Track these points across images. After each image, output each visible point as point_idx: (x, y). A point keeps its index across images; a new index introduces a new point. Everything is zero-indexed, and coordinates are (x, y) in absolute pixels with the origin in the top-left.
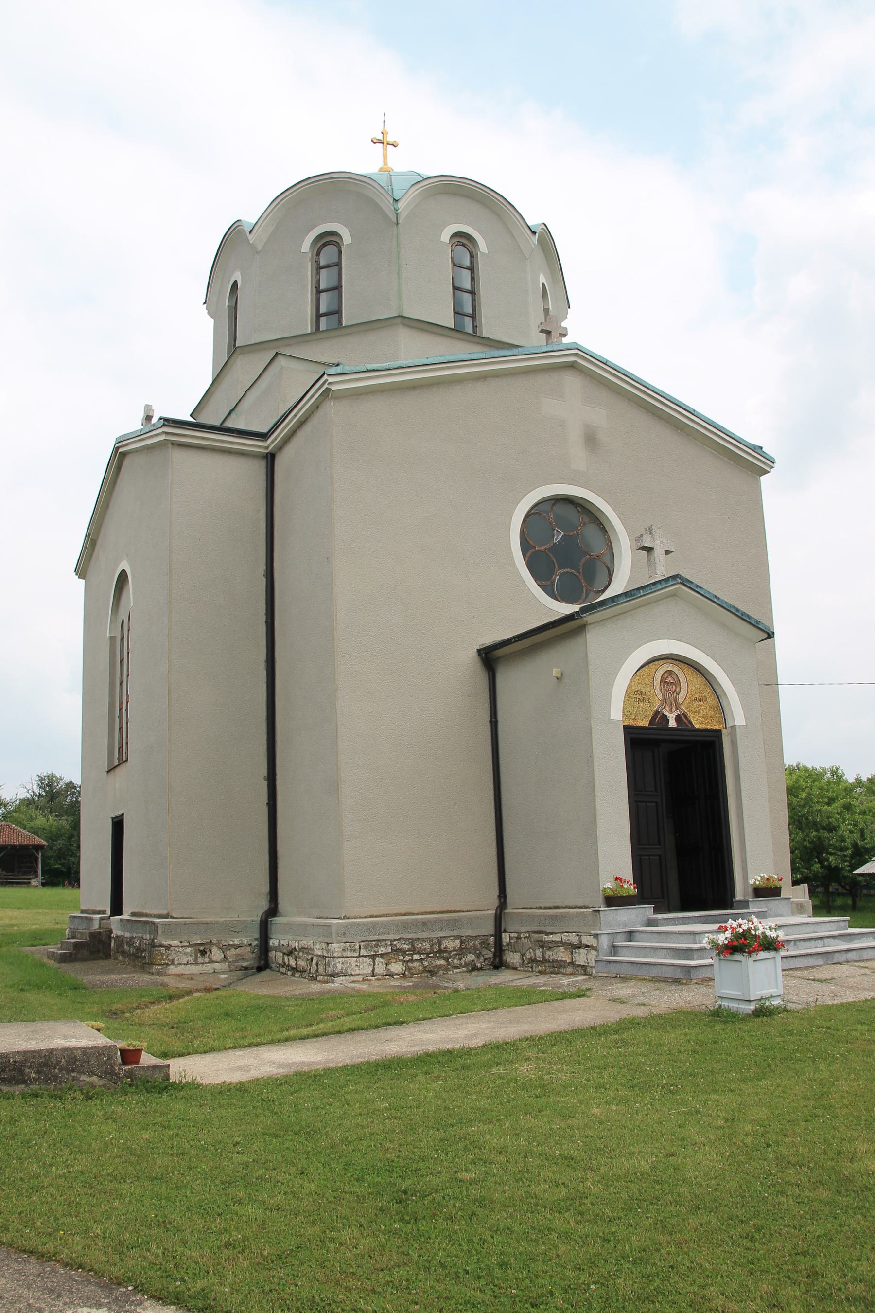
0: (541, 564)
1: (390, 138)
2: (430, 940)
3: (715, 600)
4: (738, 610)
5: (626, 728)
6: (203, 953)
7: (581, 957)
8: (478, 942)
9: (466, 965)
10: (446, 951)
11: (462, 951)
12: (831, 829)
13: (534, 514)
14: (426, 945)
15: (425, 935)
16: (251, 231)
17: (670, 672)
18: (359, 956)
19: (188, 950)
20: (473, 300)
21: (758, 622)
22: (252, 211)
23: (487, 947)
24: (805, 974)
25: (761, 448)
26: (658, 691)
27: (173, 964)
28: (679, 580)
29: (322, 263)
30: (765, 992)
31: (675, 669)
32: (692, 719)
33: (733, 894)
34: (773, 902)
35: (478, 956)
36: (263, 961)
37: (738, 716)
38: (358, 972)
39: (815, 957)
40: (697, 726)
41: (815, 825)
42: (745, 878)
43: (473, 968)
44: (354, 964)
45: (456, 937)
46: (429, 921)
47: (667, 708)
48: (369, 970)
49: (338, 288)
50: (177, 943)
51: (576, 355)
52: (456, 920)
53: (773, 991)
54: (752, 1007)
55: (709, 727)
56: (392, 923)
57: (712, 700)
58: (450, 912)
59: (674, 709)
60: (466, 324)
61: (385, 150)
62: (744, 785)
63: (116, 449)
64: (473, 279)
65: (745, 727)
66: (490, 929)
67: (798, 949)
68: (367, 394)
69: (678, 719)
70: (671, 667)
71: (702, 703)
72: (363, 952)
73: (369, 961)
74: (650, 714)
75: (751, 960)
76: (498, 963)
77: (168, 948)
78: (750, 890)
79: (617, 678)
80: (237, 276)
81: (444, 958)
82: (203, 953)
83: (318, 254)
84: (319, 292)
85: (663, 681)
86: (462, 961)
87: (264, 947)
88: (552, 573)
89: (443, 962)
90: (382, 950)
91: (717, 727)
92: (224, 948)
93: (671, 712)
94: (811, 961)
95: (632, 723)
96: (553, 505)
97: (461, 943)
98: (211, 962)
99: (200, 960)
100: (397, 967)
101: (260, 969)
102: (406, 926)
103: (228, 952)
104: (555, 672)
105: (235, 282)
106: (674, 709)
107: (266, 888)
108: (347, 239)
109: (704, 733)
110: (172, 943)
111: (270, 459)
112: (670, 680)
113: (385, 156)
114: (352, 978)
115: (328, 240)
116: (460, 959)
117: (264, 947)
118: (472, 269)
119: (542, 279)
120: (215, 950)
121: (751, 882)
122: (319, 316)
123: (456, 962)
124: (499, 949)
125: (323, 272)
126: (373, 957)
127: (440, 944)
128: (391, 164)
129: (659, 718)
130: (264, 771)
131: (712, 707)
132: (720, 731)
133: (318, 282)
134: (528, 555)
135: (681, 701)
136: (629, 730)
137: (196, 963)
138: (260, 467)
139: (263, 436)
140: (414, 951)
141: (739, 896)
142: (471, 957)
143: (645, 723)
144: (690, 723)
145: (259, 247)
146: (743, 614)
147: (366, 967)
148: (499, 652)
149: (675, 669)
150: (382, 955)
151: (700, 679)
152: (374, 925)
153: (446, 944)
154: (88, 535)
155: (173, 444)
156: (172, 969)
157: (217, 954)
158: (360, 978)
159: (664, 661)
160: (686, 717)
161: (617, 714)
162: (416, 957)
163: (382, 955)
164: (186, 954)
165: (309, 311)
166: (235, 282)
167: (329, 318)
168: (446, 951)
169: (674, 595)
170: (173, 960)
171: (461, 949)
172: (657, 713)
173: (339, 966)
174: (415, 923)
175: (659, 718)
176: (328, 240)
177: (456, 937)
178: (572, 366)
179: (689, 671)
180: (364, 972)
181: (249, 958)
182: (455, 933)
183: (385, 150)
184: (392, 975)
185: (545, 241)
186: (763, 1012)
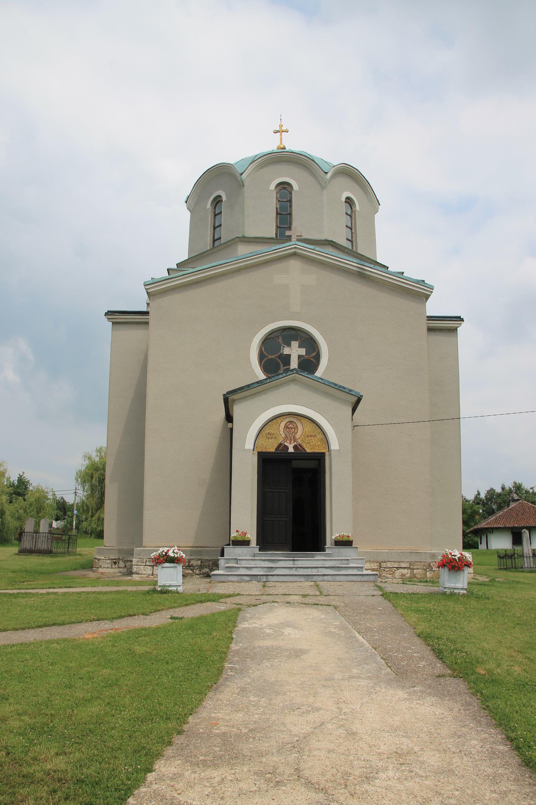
1: (284, 128)
3: (320, 380)
4: (336, 385)
8: (210, 563)
9: (203, 574)
10: (192, 566)
11: (201, 567)
13: (269, 338)
16: (242, 174)
18: (146, 565)
19: (108, 561)
21: (350, 390)
25: (423, 281)
27: (101, 567)
28: (295, 372)
30: (168, 583)
31: (295, 420)
32: (305, 447)
33: (325, 544)
34: (344, 549)
37: (334, 445)
38: (144, 573)
39: (299, 577)
40: (308, 451)
42: (332, 535)
44: (143, 569)
45: (198, 560)
47: (288, 441)
48: (151, 572)
50: (103, 558)
51: (295, 248)
52: (199, 551)
55: (317, 451)
57: (321, 436)
58: (202, 547)
59: (292, 442)
61: (281, 135)
62: (334, 483)
67: (298, 572)
68: (169, 290)
69: (295, 447)
70: (288, 420)
71: (312, 438)
72: (148, 563)
73: (150, 568)
77: (99, 560)
78: (333, 542)
81: (191, 570)
82: (115, 563)
83: (215, 208)
85: (286, 427)
86: (201, 572)
89: (190, 571)
91: (323, 451)
93: (290, 443)
95: (264, 450)
96: (283, 332)
97: (201, 562)
98: (119, 567)
99: (113, 566)
103: (127, 564)
106: (292, 442)
108: (224, 198)
109: (312, 455)
110: (101, 558)
112: (291, 426)
113: (281, 139)
114: (141, 576)
115: (284, 187)
116: (200, 571)
120: (121, 562)
123: (198, 572)
126: (153, 566)
127: (189, 562)
128: (285, 143)
129: (282, 447)
132: (324, 453)
134: (263, 361)
135: (297, 437)
137: (112, 568)
143: (273, 450)
144: (304, 449)
146: (340, 386)
149: (295, 420)
153: (192, 562)
156: (101, 570)
158: (146, 576)
159: (287, 416)
160: (301, 446)
161: (249, 445)
164: (107, 563)
168: (192, 566)
169: (293, 381)
170: (101, 566)
171: (201, 565)
172: (281, 444)
176: (349, 201)
177: (198, 560)
178: (294, 255)
179: (268, 426)
180: (147, 573)
182: (199, 557)
183: (281, 135)
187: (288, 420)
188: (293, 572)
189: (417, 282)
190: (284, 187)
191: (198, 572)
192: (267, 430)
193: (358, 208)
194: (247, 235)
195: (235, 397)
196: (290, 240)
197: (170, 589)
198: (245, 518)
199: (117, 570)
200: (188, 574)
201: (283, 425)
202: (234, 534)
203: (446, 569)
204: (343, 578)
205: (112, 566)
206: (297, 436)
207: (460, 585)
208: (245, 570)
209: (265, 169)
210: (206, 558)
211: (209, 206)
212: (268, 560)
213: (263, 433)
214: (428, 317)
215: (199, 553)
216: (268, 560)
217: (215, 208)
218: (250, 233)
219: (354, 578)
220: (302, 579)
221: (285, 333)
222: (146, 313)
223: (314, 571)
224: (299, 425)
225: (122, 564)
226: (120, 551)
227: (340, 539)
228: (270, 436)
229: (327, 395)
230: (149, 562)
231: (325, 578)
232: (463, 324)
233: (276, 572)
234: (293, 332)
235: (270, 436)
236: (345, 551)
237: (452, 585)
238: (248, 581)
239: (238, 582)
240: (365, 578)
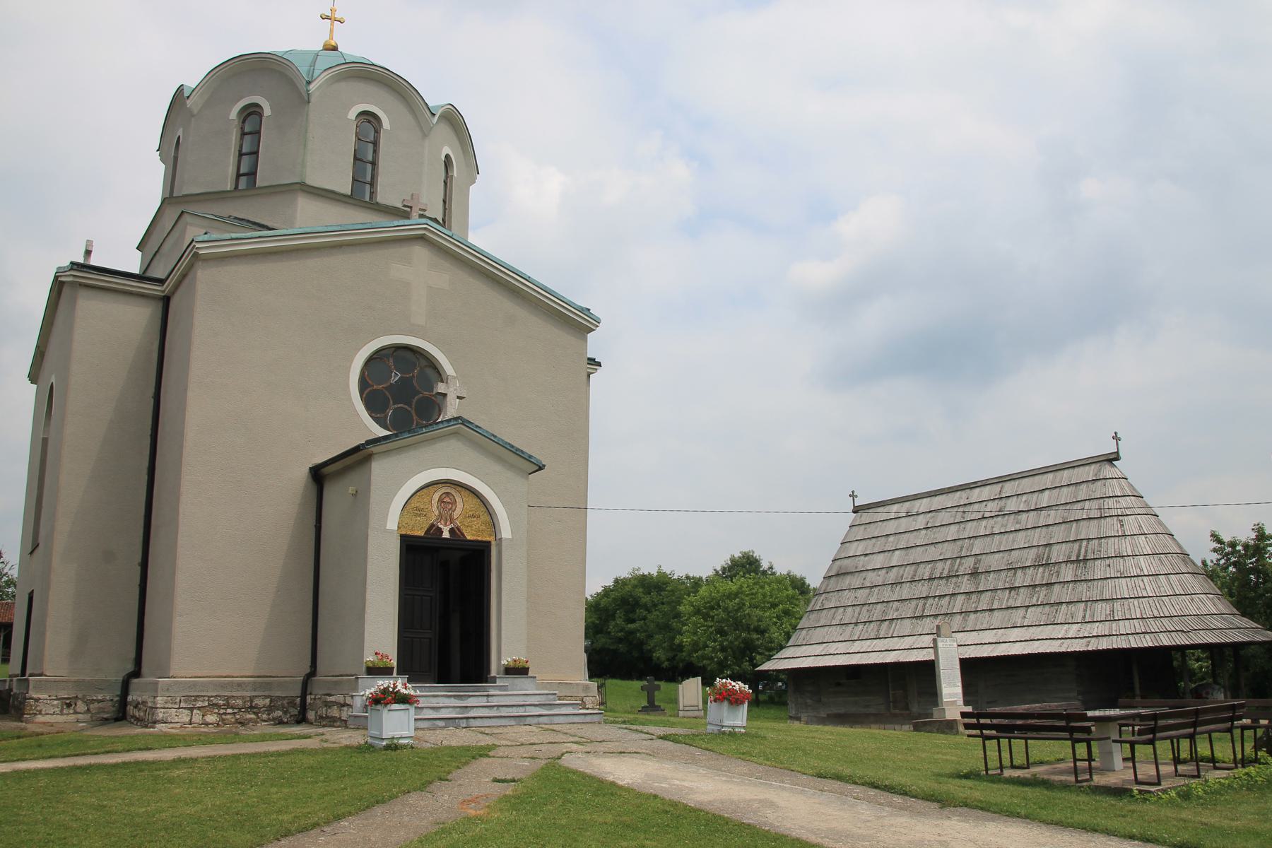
0: (374, 402)
1: (338, 16)
2: (243, 698)
5: (402, 536)
6: (69, 705)
7: (345, 714)
9: (274, 719)
11: (270, 709)
12: (762, 632)
14: (240, 702)
15: (239, 694)
17: (448, 494)
20: (373, 170)
21: (530, 456)
22: (192, 79)
23: (294, 705)
24: (487, 731)
26: (435, 508)
29: (247, 130)
30: (397, 734)
33: (489, 671)
35: (285, 713)
36: (121, 713)
37: (506, 532)
40: (469, 538)
41: (748, 629)
42: (499, 659)
43: (280, 722)
45: (266, 697)
46: (244, 683)
49: (256, 153)
52: (268, 683)
53: (405, 733)
54: (384, 743)
56: (210, 682)
57: (485, 517)
60: (362, 191)
63: (56, 277)
64: (375, 151)
65: (511, 540)
66: (297, 692)
69: (452, 531)
72: (183, 705)
73: (187, 712)
74: (426, 527)
75: (385, 711)
76: (301, 719)
77: (37, 700)
79: (397, 497)
80: (180, 132)
83: (244, 122)
84: (241, 155)
85: (441, 500)
87: (123, 703)
88: (387, 407)
89: (253, 716)
90: (199, 704)
92: (88, 702)
94: (503, 722)
95: (409, 533)
98: (76, 713)
100: (211, 718)
101: (116, 720)
102: (223, 686)
104: (351, 490)
105: (447, 156)
107: (133, 655)
108: (267, 111)
111: (166, 301)
112: (447, 500)
113: (331, 31)
115: (252, 112)
117: (123, 703)
118: (375, 143)
119: (446, 150)
120: (80, 703)
121: (504, 662)
122: (239, 175)
123: (265, 716)
124: (304, 708)
125: (247, 138)
126: (191, 709)
127: (251, 701)
129: (434, 530)
130: (139, 558)
131: (484, 523)
132: (489, 542)
133: (241, 146)
136: (404, 538)
138: (160, 305)
139: (161, 282)
140: (228, 706)
141: (493, 673)
142: (279, 713)
143: (421, 533)
145: (195, 112)
147: (184, 717)
148: (327, 470)
150: (199, 708)
151: (476, 500)
152: (195, 684)
153: (256, 701)
154: (38, 347)
155: (81, 285)
156: (40, 718)
157: (81, 706)
161: (392, 523)
162: (229, 711)
163: (199, 708)
165: (231, 171)
166: (447, 156)
167: (247, 176)
169: (455, 433)
172: (432, 525)
173: (161, 715)
174: (231, 684)
175: (434, 530)
178: (422, 238)
181: (110, 710)
182: (266, 693)
184: (207, 724)
185: (453, 119)
186: (393, 747)
187: (443, 490)
188: (494, 713)
189: (582, 310)
190: (252, 112)
191: (265, 716)
192: (414, 504)
193: (386, 124)
194: (309, 182)
195: (375, 449)
196: (408, 218)
197: (401, 741)
198: (380, 632)
199: (72, 718)
200: (250, 720)
201: (436, 497)
202: (369, 658)
203: (726, 703)
204: (562, 719)
205: (62, 710)
206: (455, 515)
207: (739, 723)
208: (431, 711)
209: (343, 85)
210: (278, 694)
211: (234, 114)
212: (454, 696)
213: (408, 507)
214: (589, 359)
215: (268, 686)
216: (454, 696)
217: (244, 122)
218: (314, 180)
219: (576, 719)
220: (513, 722)
221: (400, 352)
222: (1112, 459)
223: (520, 711)
224: (458, 500)
225: (81, 706)
226: (78, 684)
227: (512, 664)
228: (419, 512)
229: (500, 459)
230: (186, 701)
231: (541, 719)
232: (600, 370)
233: (472, 714)
234: (409, 355)
235: (419, 512)
236: (519, 682)
237: (731, 723)
238: (443, 728)
239: (429, 729)
240: (588, 719)
